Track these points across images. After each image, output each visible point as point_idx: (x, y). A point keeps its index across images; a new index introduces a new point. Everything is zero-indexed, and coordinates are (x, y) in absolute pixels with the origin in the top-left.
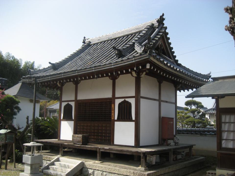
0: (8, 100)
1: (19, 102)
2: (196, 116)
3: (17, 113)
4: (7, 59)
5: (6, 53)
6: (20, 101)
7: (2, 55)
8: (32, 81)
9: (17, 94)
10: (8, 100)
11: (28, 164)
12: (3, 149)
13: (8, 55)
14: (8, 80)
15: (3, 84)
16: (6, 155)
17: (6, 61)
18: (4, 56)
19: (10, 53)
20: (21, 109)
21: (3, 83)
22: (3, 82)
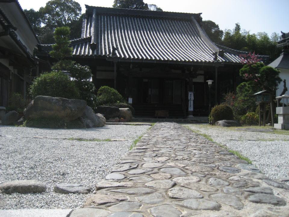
0: (267, 70)
1: (279, 72)
2: (53, 180)
3: (278, 84)
4: (273, 41)
5: (272, 34)
6: (280, 71)
7: (268, 38)
8: (287, 44)
9: (278, 66)
10: (267, 70)
11: (280, 115)
12: (261, 109)
13: (274, 36)
14: (269, 57)
15: (266, 62)
16: (266, 90)
17: (273, 44)
18: (270, 38)
19: (277, 34)
20: (288, 90)
21: (265, 61)
22: (266, 60)
